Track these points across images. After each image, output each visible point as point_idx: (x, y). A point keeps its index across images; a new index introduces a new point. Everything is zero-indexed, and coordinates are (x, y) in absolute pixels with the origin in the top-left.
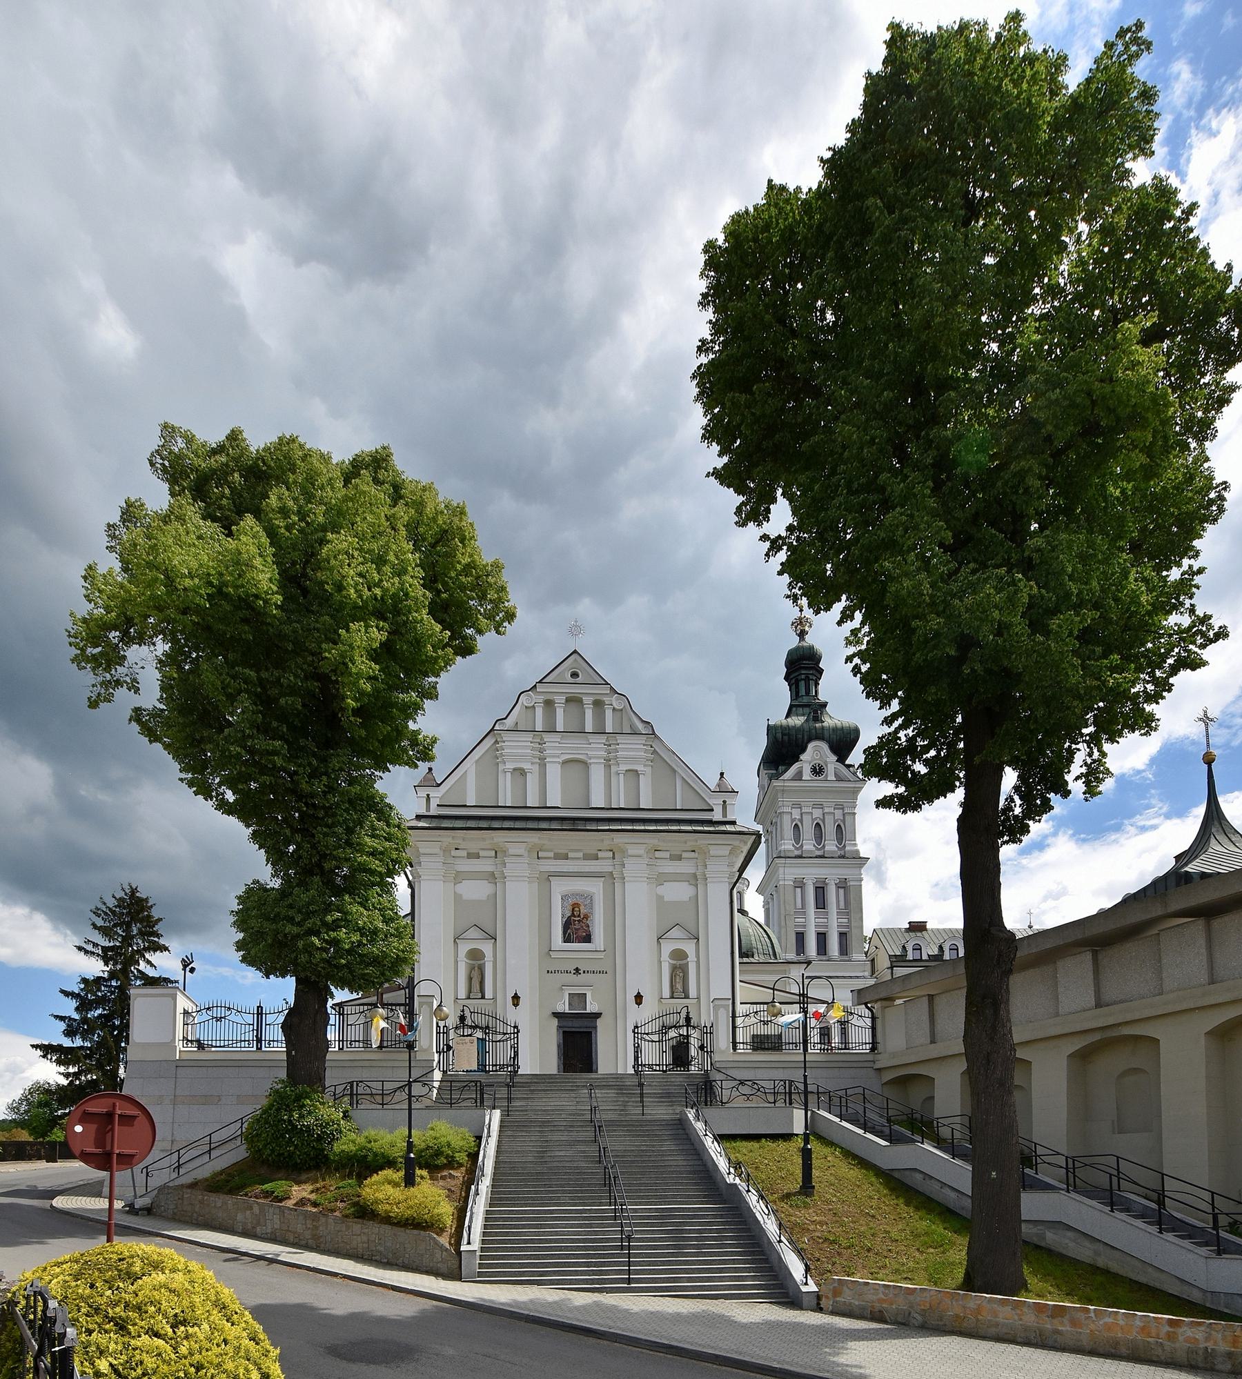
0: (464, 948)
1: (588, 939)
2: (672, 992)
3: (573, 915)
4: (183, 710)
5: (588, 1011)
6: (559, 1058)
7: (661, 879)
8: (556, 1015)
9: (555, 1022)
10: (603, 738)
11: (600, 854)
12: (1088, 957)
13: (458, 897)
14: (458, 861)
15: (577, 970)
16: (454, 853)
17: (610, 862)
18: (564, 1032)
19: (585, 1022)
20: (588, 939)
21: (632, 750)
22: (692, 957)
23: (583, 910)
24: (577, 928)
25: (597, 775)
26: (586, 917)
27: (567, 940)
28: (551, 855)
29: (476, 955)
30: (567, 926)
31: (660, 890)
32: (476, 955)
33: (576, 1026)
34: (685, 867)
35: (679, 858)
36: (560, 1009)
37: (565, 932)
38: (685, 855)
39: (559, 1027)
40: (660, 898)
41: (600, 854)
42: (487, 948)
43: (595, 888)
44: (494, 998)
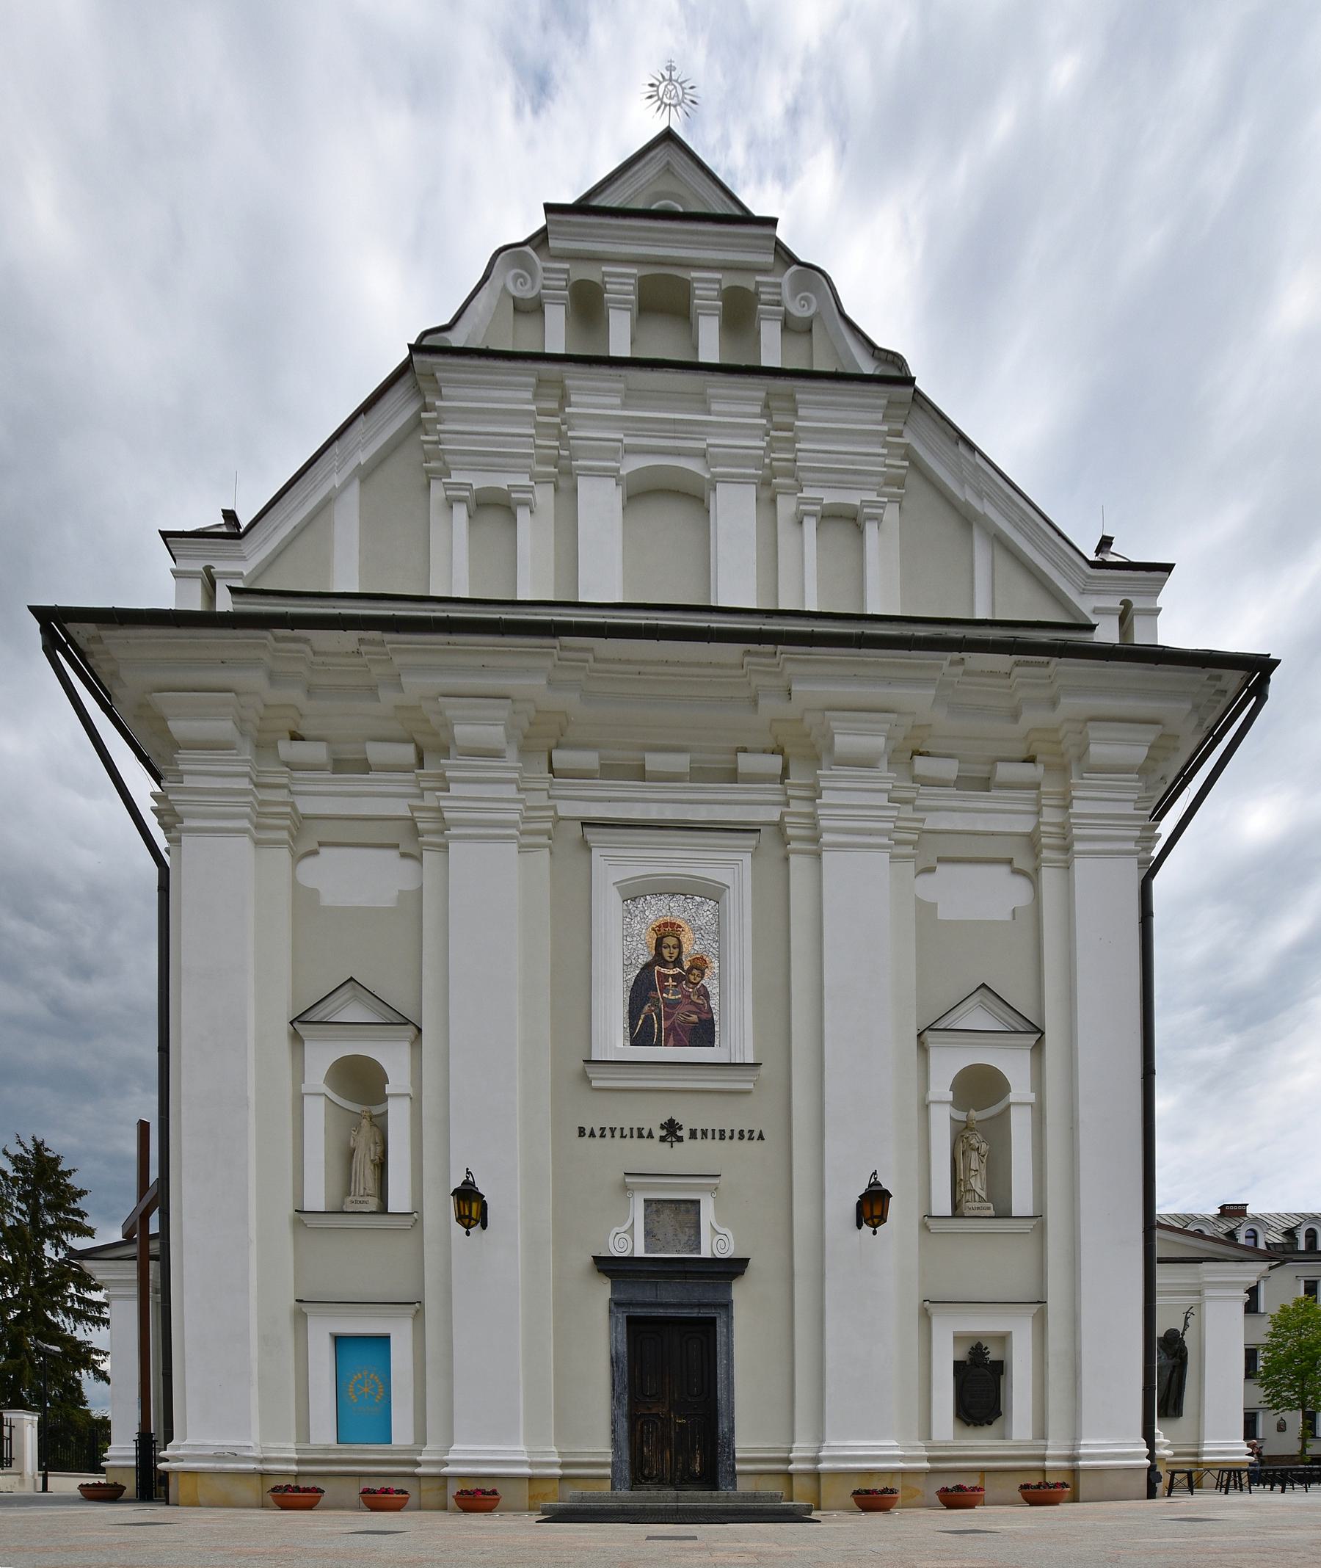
0: (948, 1064)
1: (703, 1033)
2: (955, 1205)
3: (659, 959)
4: (693, 315)
5: (705, 1253)
6: (615, 1397)
7: (305, 837)
8: (607, 1266)
9: (603, 1290)
10: (756, 389)
11: (747, 763)
12: (409, 1090)
13: (304, 900)
14: (927, 797)
15: (671, 1130)
16: (289, 750)
17: (771, 792)
18: (631, 1321)
19: (699, 1292)
20: (703, 1033)
21: (839, 431)
22: (1020, 1089)
23: (691, 947)
24: (669, 1002)
25: (734, 509)
26: (699, 966)
27: (640, 1036)
28: (589, 759)
29: (980, 1088)
30: (641, 991)
31: (928, 888)
32: (980, 1088)
33: (670, 1299)
34: (1004, 817)
35: (986, 784)
36: (618, 1248)
37: (633, 1015)
38: (1005, 771)
39: (616, 1304)
40: (925, 910)
41: (747, 763)
42: (1013, 1065)
43: (733, 869)
44: (1039, 1217)
